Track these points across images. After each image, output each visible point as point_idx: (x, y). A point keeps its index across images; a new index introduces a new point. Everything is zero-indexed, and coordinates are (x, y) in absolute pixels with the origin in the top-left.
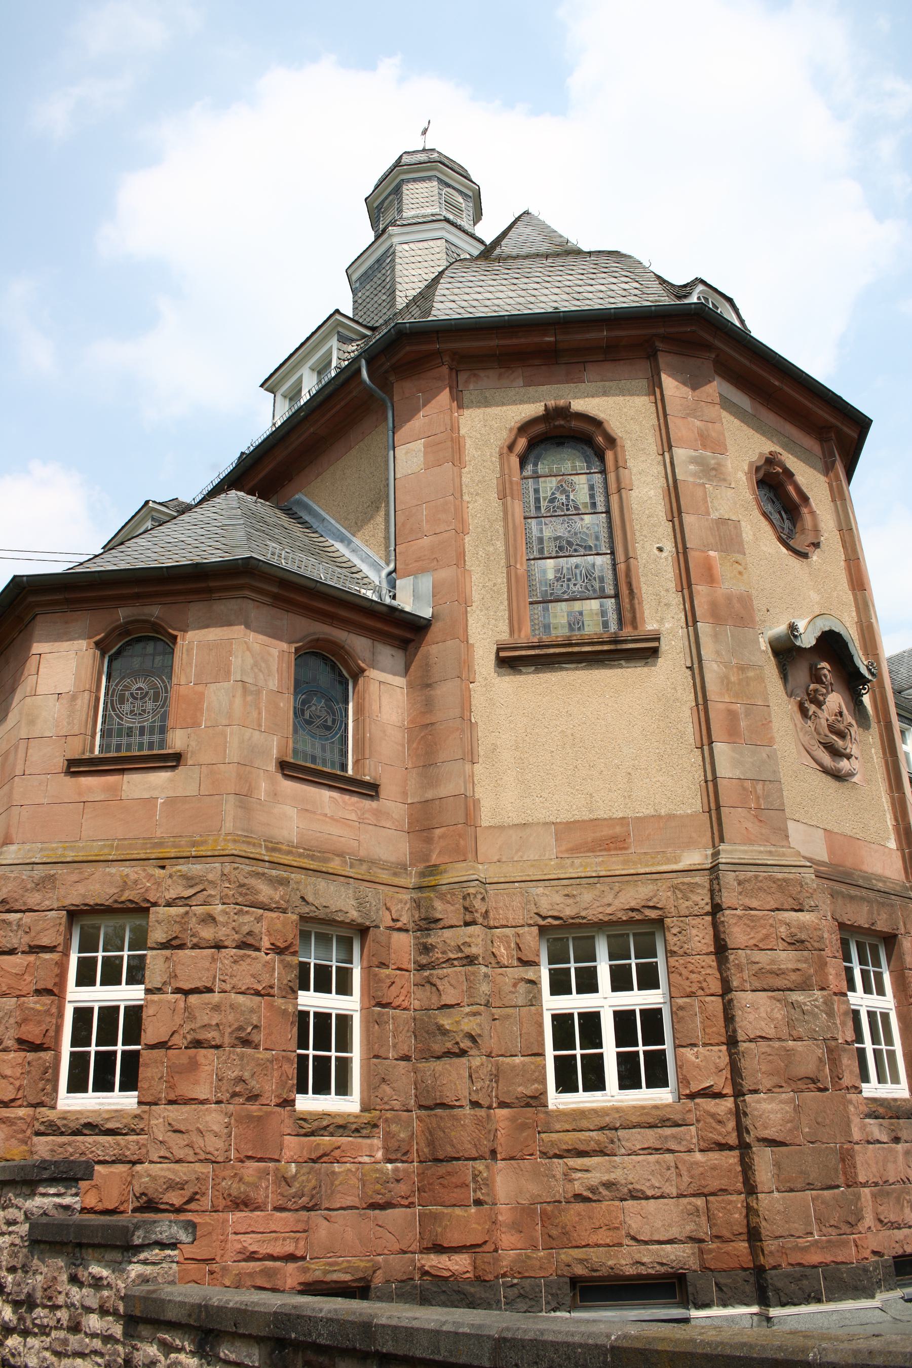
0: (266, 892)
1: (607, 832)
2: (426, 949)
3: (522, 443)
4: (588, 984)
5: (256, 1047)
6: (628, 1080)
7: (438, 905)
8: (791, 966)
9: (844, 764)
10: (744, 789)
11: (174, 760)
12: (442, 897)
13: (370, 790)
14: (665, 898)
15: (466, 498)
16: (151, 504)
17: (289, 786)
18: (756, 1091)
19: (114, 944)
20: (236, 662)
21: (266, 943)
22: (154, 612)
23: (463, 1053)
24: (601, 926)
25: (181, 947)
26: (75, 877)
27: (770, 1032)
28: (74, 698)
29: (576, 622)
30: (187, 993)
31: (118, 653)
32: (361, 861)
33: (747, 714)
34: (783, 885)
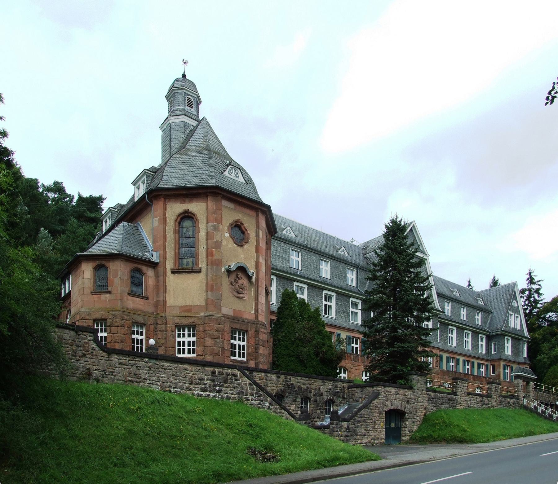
0: (126, 317)
1: (188, 308)
2: (156, 328)
3: (179, 218)
4: (184, 336)
5: (125, 343)
6: (189, 353)
7: (158, 321)
8: (216, 334)
9: (241, 295)
10: (213, 301)
11: (110, 293)
12: (159, 319)
13: (147, 298)
14: (196, 321)
15: (167, 233)
16: (110, 208)
17: (130, 298)
18: (207, 355)
19: (102, 326)
20: (119, 273)
21: (126, 326)
22: (104, 262)
23: (161, 346)
24: (187, 326)
25: (112, 326)
26: (94, 314)
27: (211, 345)
28: (91, 279)
29: (187, 264)
30: (113, 334)
31: (98, 270)
32: (145, 312)
33: (216, 285)
34: (217, 320)
